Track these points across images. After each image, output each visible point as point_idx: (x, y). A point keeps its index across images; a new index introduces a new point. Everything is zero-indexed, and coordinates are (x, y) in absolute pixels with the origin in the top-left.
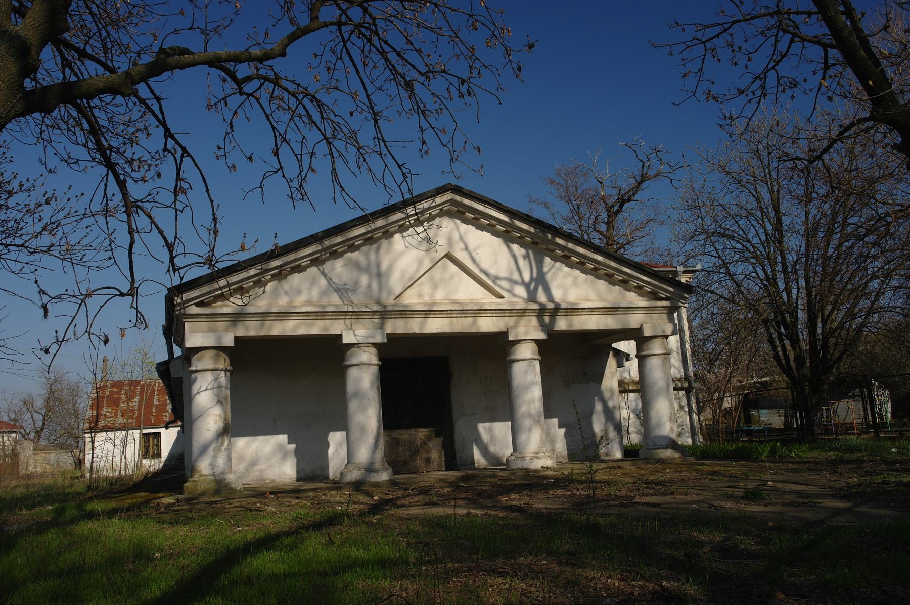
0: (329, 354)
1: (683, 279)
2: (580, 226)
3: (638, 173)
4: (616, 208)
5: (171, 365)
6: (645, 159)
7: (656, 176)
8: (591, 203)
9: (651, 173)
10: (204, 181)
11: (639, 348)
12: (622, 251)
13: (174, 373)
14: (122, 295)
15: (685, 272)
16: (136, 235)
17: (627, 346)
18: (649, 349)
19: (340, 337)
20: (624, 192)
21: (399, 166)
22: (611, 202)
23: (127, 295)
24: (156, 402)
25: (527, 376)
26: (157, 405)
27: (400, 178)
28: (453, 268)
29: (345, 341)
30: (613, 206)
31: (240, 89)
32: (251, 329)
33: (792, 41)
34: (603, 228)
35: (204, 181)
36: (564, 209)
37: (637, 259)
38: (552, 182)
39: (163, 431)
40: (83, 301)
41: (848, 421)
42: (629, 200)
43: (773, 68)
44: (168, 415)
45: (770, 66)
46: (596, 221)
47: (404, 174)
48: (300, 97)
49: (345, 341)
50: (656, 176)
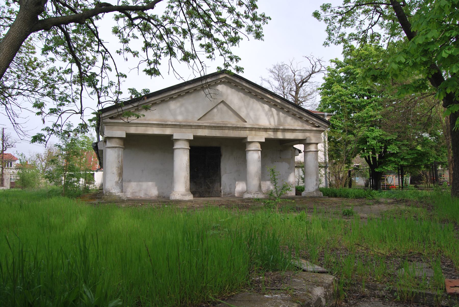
0: (165, 144)
1: (327, 119)
2: (284, 92)
3: (310, 70)
4: (300, 85)
5: (98, 144)
6: (314, 64)
7: (318, 72)
8: (289, 83)
9: (316, 70)
10: (115, 64)
11: (305, 148)
12: (301, 104)
13: (100, 148)
14: (77, 113)
15: (328, 115)
16: (83, 86)
17: (301, 147)
18: (309, 149)
19: (172, 136)
20: (304, 78)
21: (201, 63)
22: (298, 82)
23: (79, 113)
24: (92, 160)
25: (254, 157)
26: (93, 161)
27: (200, 68)
28: (225, 108)
29: (174, 138)
30: (299, 84)
31: (132, 22)
32: (133, 130)
33: (380, 17)
34: (294, 93)
35: (115, 64)
36: (276, 84)
37: (307, 108)
38: (272, 72)
39: (95, 172)
40: (60, 115)
41: (392, 184)
42: (306, 82)
43: (371, 28)
44: (98, 166)
45: (370, 27)
46: (291, 90)
47: (202, 66)
48: (158, 27)
49: (174, 138)
50: (318, 72)
